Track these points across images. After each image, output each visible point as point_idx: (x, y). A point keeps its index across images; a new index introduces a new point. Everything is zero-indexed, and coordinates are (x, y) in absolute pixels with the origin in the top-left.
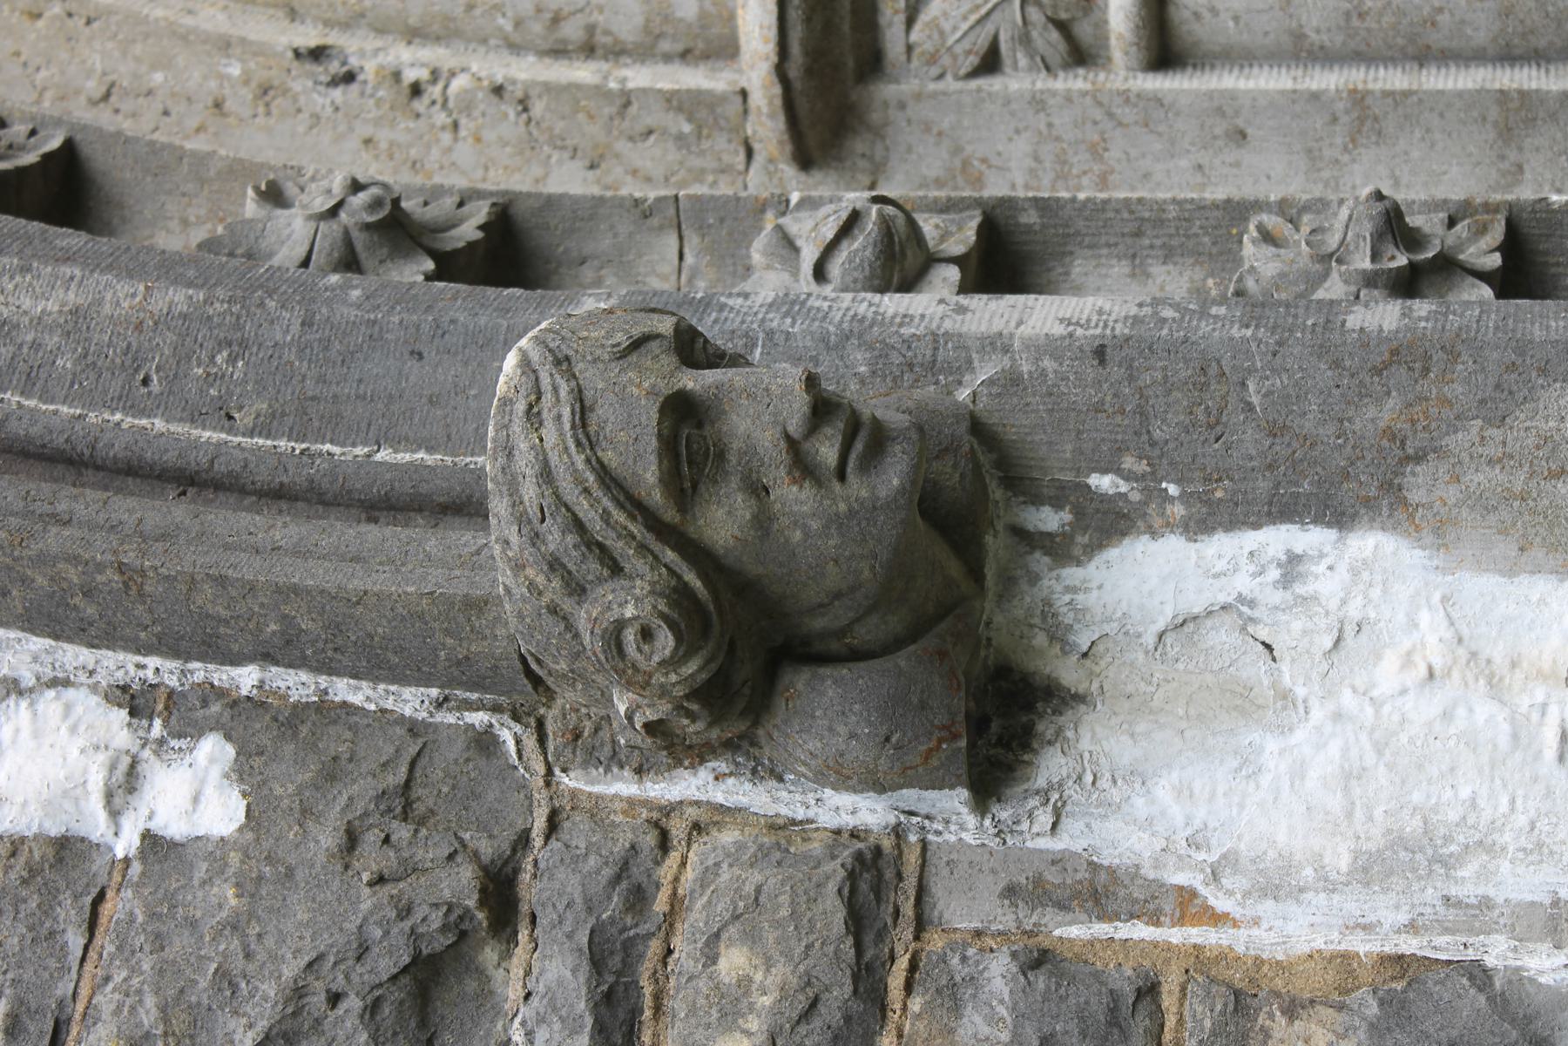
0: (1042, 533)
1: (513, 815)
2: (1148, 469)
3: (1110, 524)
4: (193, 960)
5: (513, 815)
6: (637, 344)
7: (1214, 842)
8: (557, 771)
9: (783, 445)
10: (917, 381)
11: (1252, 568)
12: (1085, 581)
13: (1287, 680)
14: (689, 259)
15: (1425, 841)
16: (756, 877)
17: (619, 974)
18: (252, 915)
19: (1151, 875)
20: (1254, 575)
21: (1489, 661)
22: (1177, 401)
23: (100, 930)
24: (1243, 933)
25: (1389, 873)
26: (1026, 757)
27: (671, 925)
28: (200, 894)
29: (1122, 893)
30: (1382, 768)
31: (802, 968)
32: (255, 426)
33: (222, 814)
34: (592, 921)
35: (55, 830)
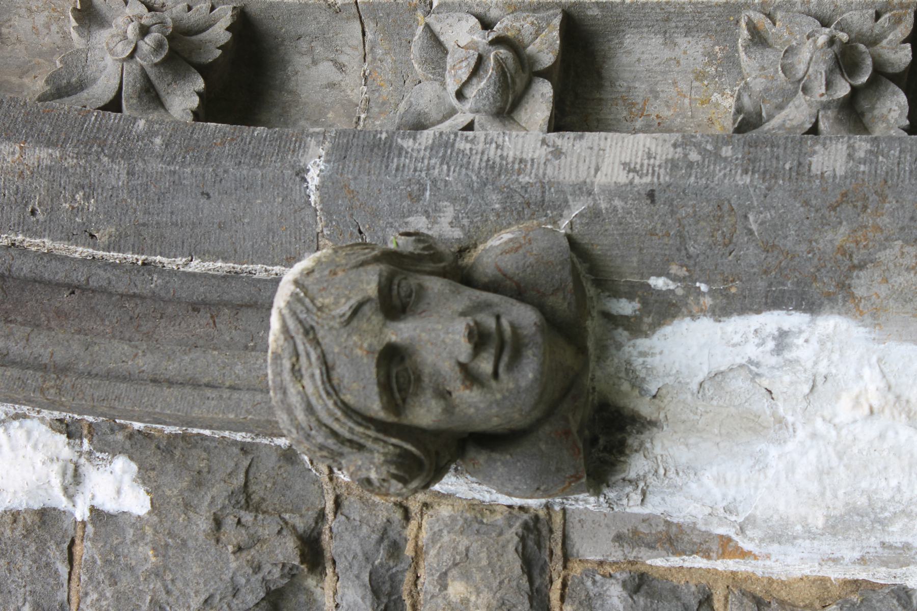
0: (622, 316)
1: (312, 499)
2: (687, 274)
3: (665, 310)
4: (135, 592)
5: (312, 499)
6: (356, 311)
7: (740, 509)
8: (335, 470)
9: (457, 369)
10: (533, 214)
11: (757, 341)
12: (651, 348)
13: (781, 411)
14: (369, 36)
15: (870, 510)
16: (464, 542)
17: (390, 595)
18: (165, 567)
19: (703, 528)
20: (758, 345)
21: (908, 402)
22: (704, 228)
23: (76, 563)
24: (760, 563)
25: (848, 529)
26: (622, 459)
27: (417, 563)
28: (132, 549)
29: (686, 539)
30: (842, 468)
31: (498, 595)
32: (110, 244)
33: (136, 502)
34: (369, 567)
35: (37, 506)
